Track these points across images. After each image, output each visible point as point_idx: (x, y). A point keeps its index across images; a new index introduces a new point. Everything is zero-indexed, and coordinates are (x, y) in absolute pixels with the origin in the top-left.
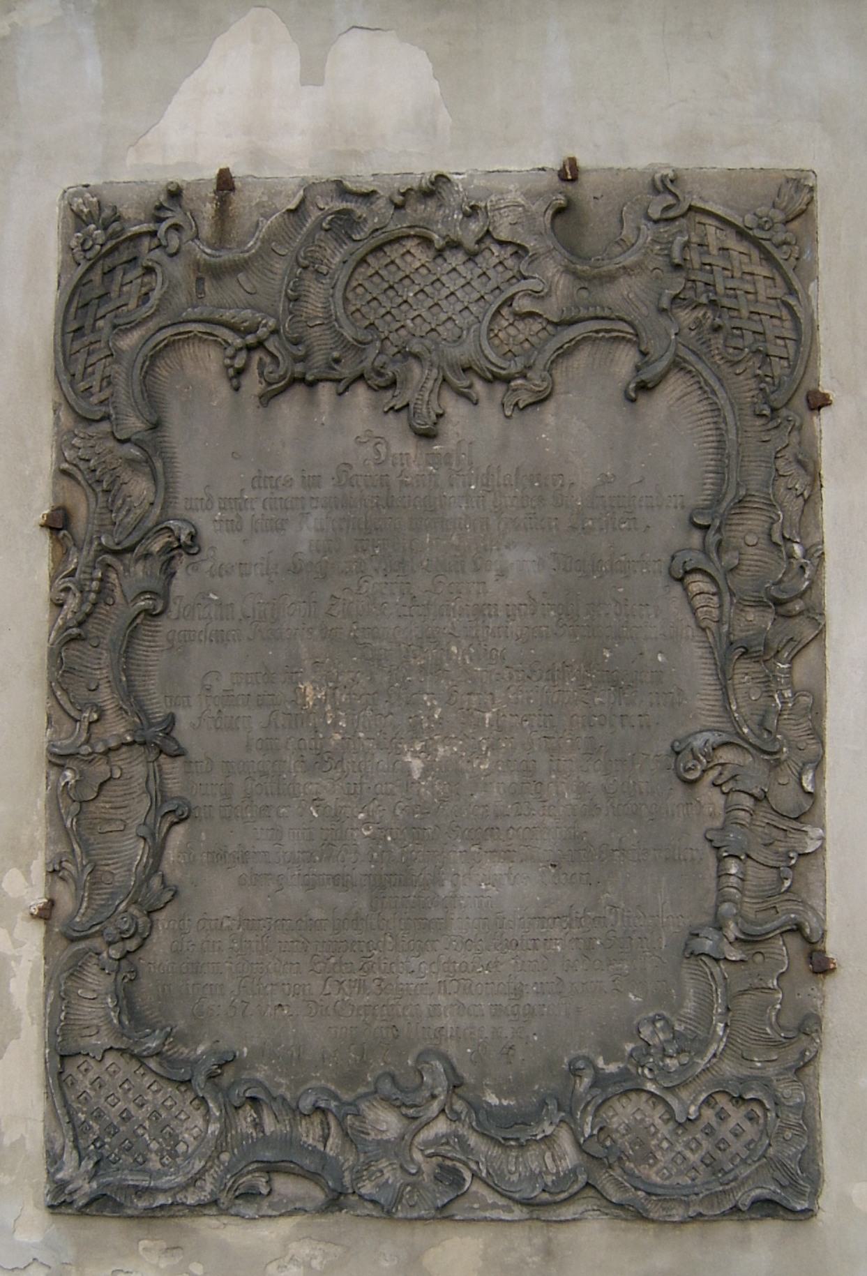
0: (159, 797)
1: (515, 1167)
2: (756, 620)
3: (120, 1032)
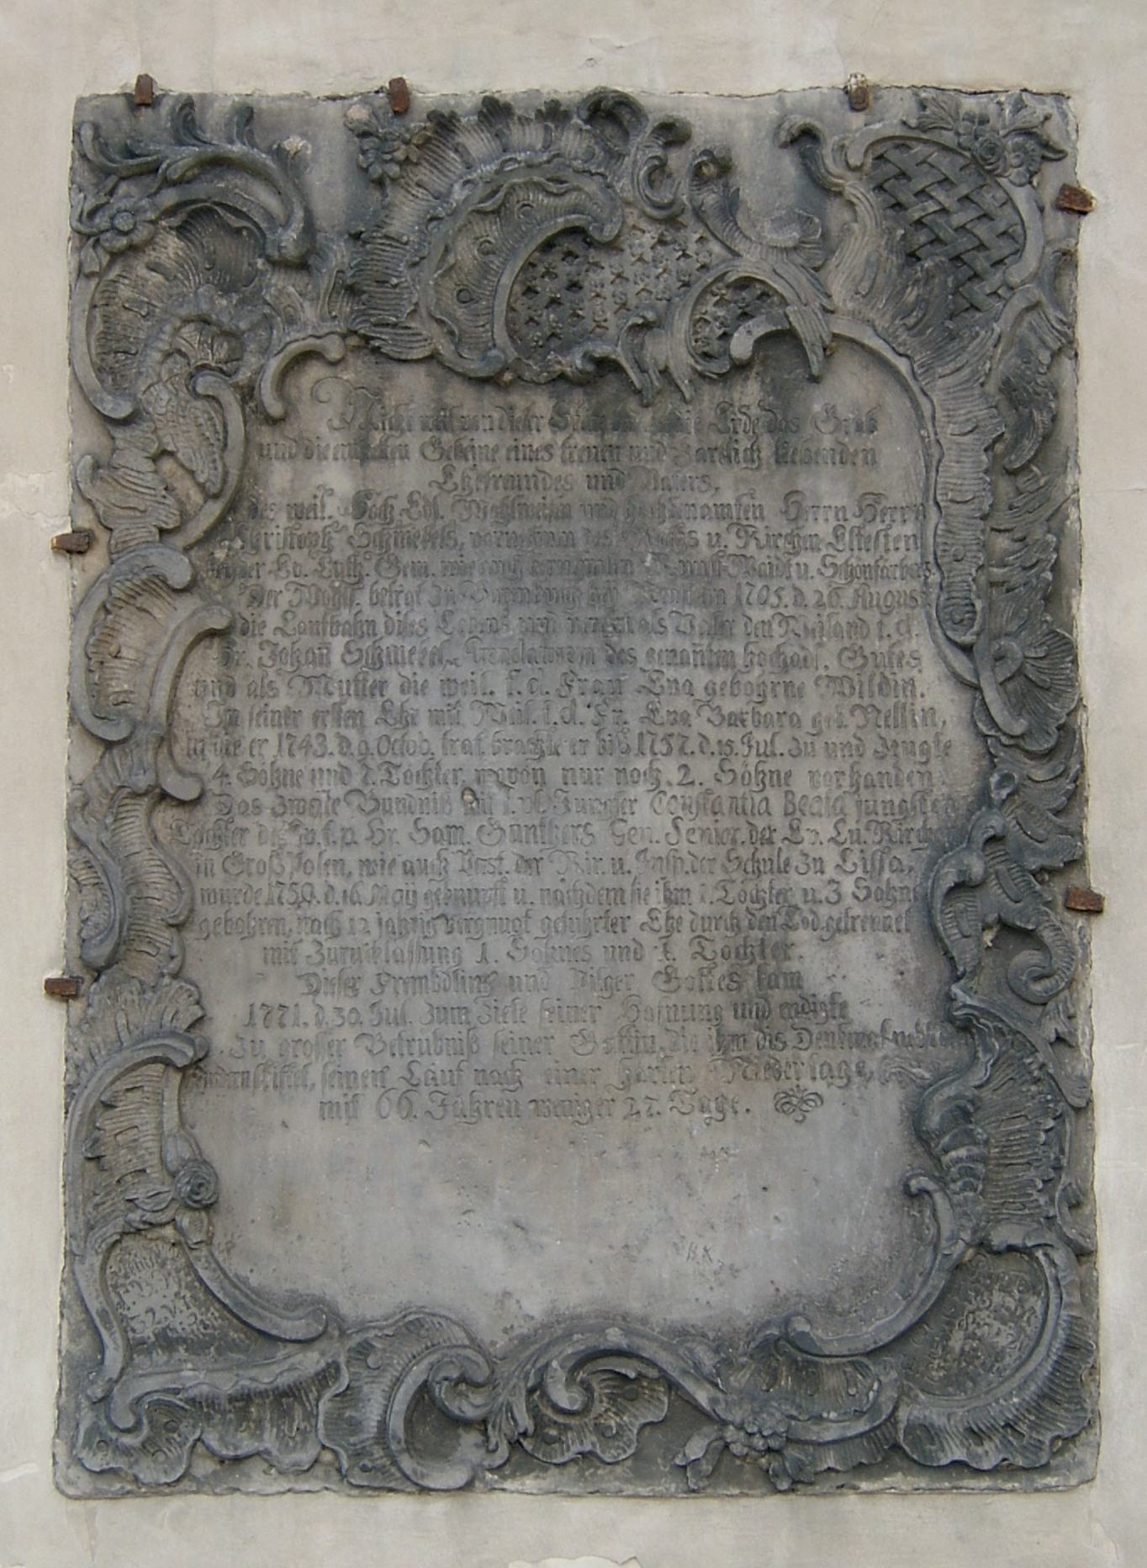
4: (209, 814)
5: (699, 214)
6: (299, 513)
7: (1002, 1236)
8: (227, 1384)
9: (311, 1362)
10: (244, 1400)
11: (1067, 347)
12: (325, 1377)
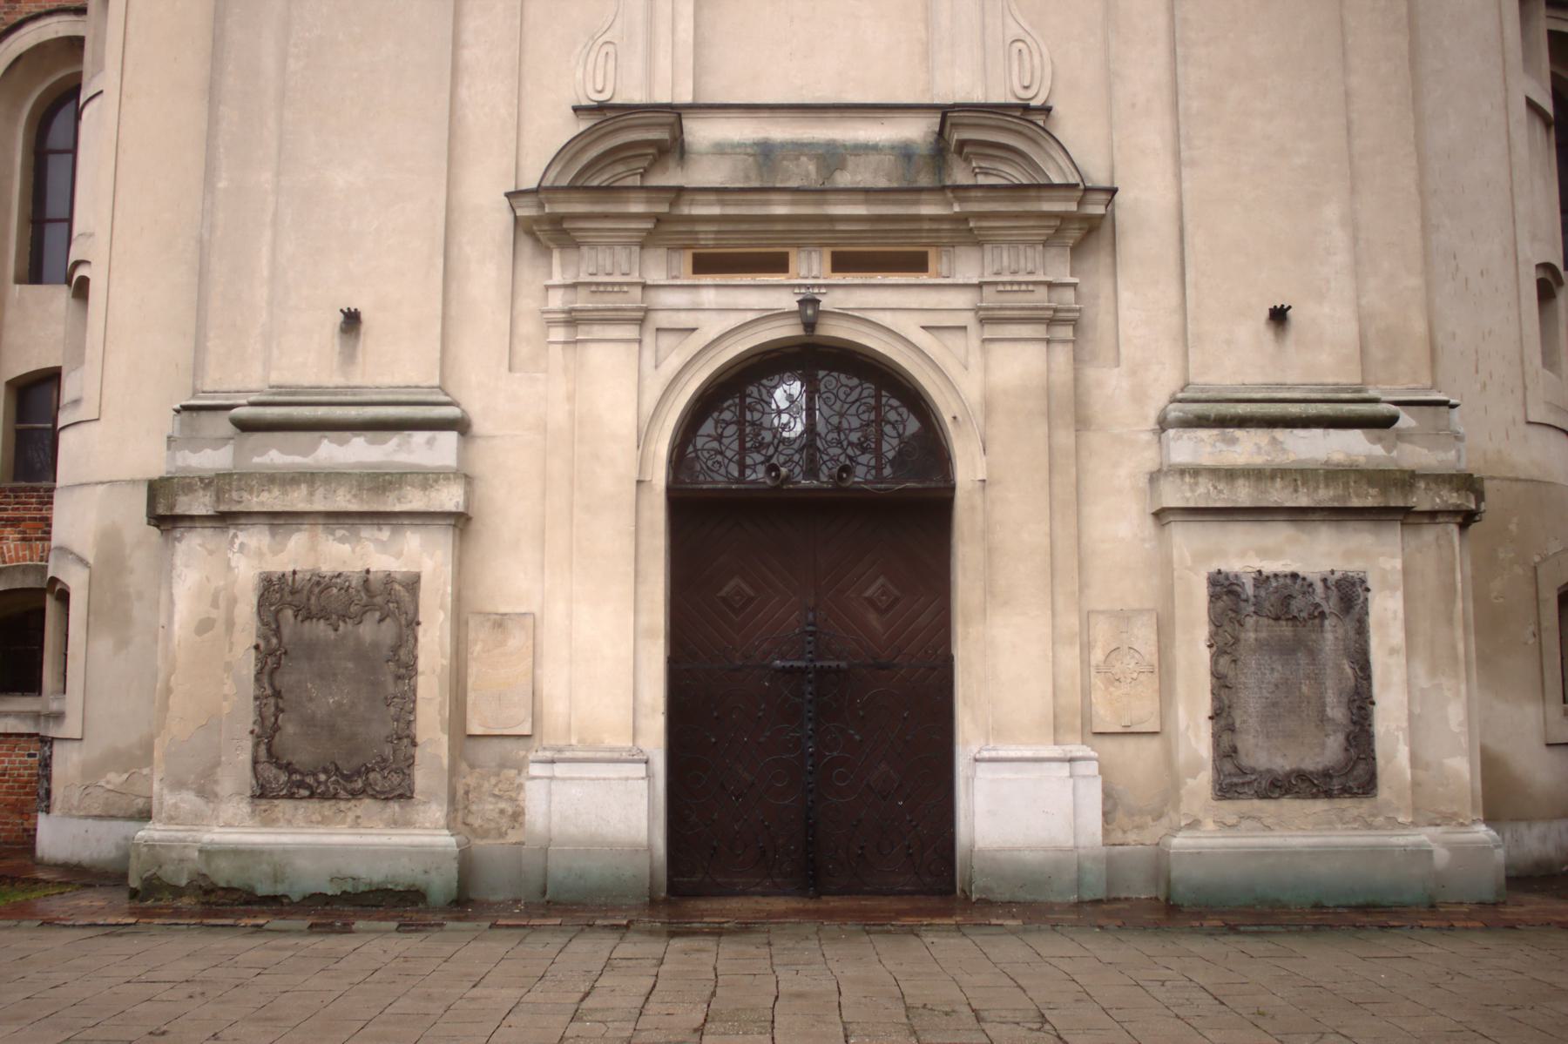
0: (277, 707)
1: (349, 786)
2: (403, 671)
3: (268, 757)
4: (1234, 690)
5: (1309, 592)
6: (1246, 640)
7: (1362, 756)
8: (1241, 781)
9: (1253, 777)
10: (1243, 784)
11: (1367, 614)
12: (1255, 780)
